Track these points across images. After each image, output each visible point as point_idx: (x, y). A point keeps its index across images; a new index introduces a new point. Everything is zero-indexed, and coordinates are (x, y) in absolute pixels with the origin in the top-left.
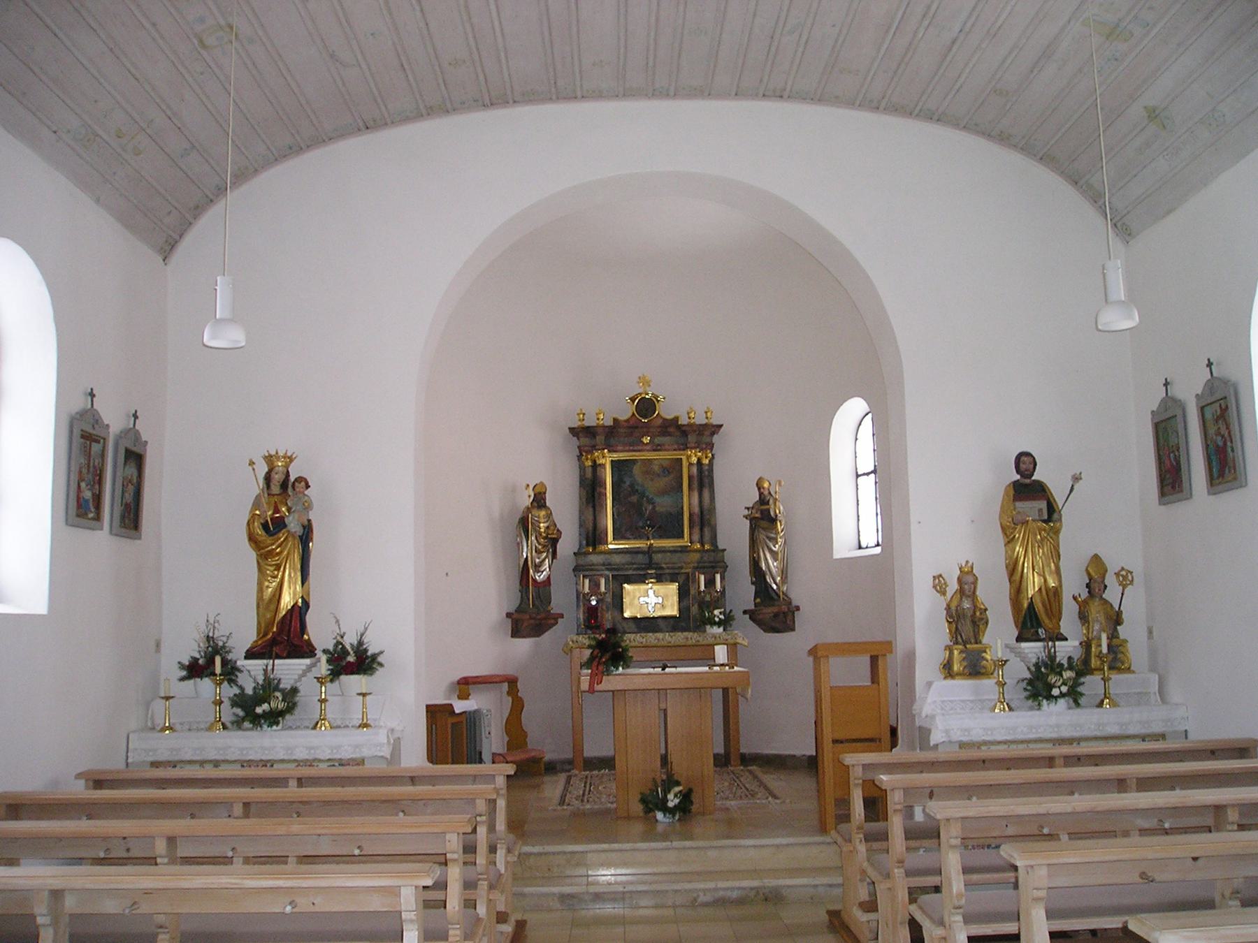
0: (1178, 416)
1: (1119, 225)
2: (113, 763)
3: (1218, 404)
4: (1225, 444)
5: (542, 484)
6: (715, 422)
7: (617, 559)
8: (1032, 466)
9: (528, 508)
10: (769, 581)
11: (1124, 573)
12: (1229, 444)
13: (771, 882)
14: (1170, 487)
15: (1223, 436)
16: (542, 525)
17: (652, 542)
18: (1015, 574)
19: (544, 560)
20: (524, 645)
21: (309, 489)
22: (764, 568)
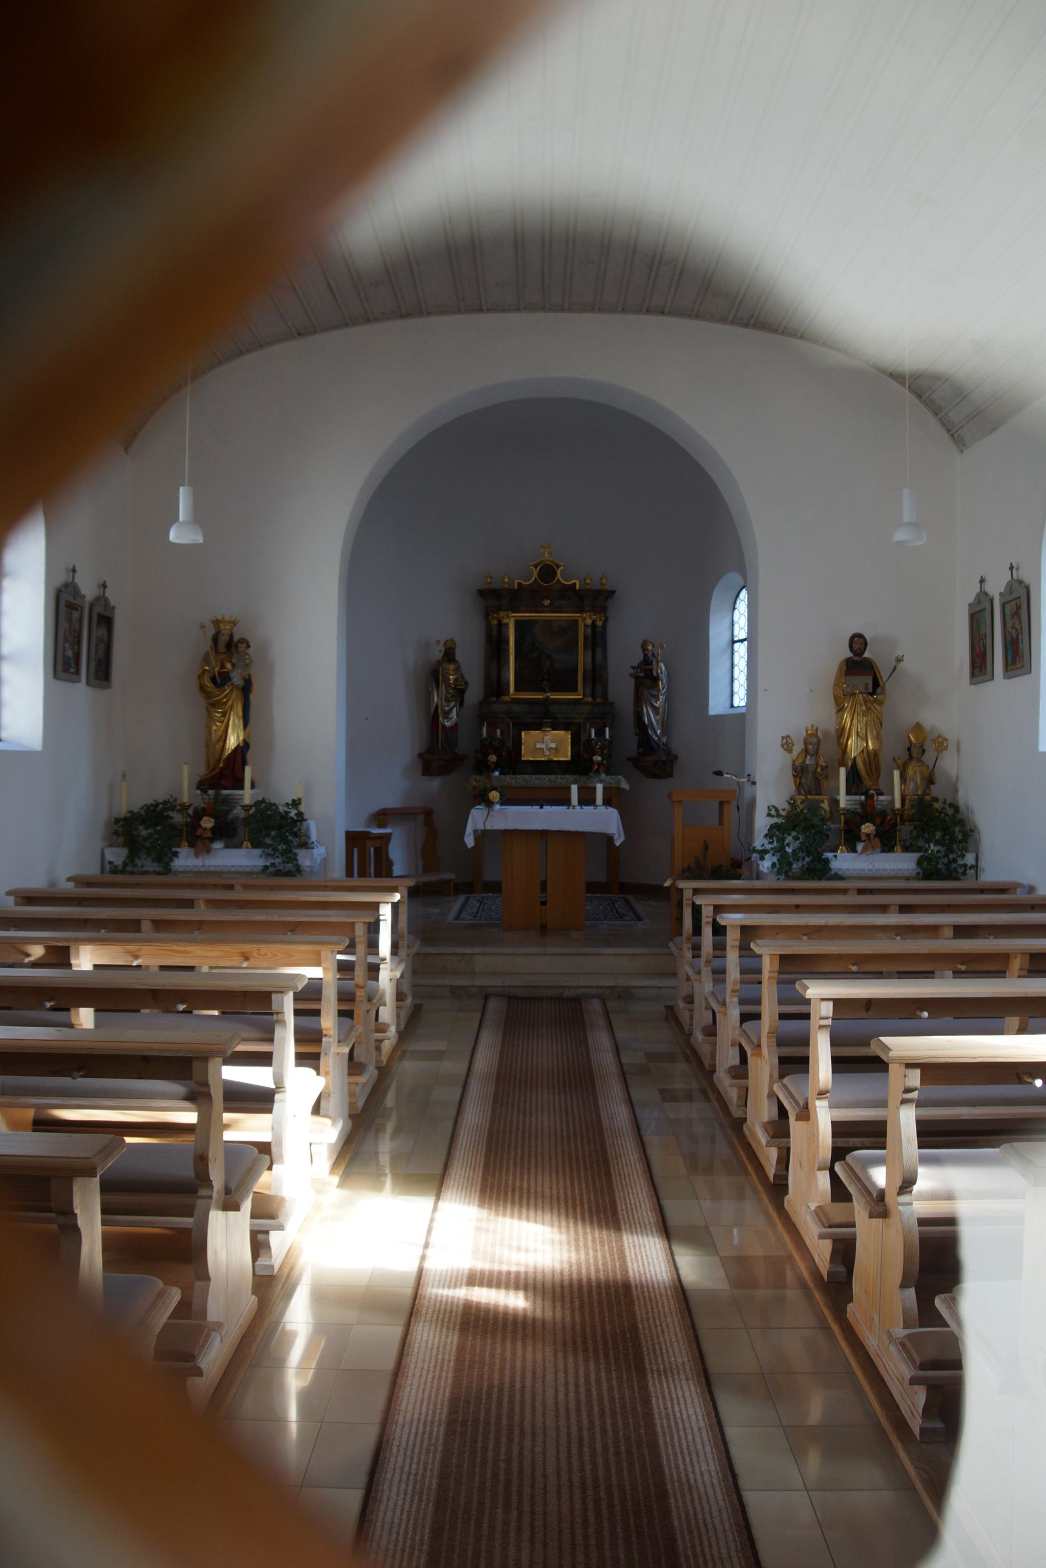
0: (1022, 598)
1: (955, 436)
2: (37, 882)
3: (1014, 602)
4: (1018, 636)
5: (452, 640)
6: (609, 588)
7: (516, 708)
8: (863, 646)
9: (438, 661)
10: (650, 733)
11: (940, 740)
12: (1020, 636)
13: (624, 982)
14: (978, 669)
15: (1016, 630)
16: (451, 677)
17: (549, 694)
18: (843, 737)
19: (452, 708)
20: (434, 784)
21: (250, 649)
22: (646, 722)
